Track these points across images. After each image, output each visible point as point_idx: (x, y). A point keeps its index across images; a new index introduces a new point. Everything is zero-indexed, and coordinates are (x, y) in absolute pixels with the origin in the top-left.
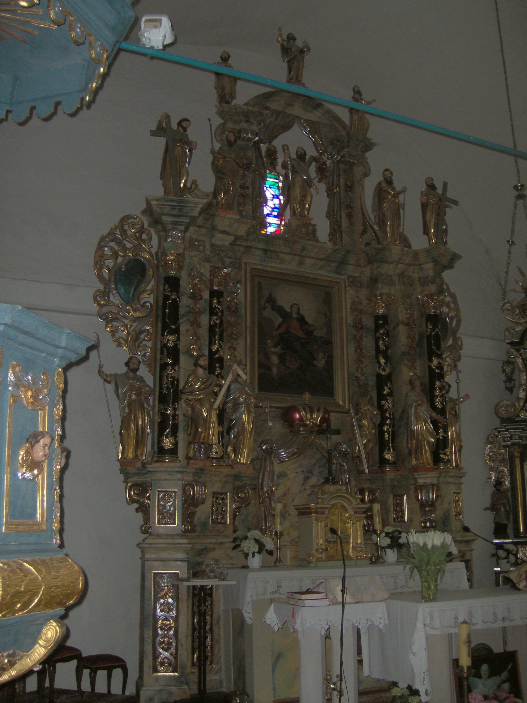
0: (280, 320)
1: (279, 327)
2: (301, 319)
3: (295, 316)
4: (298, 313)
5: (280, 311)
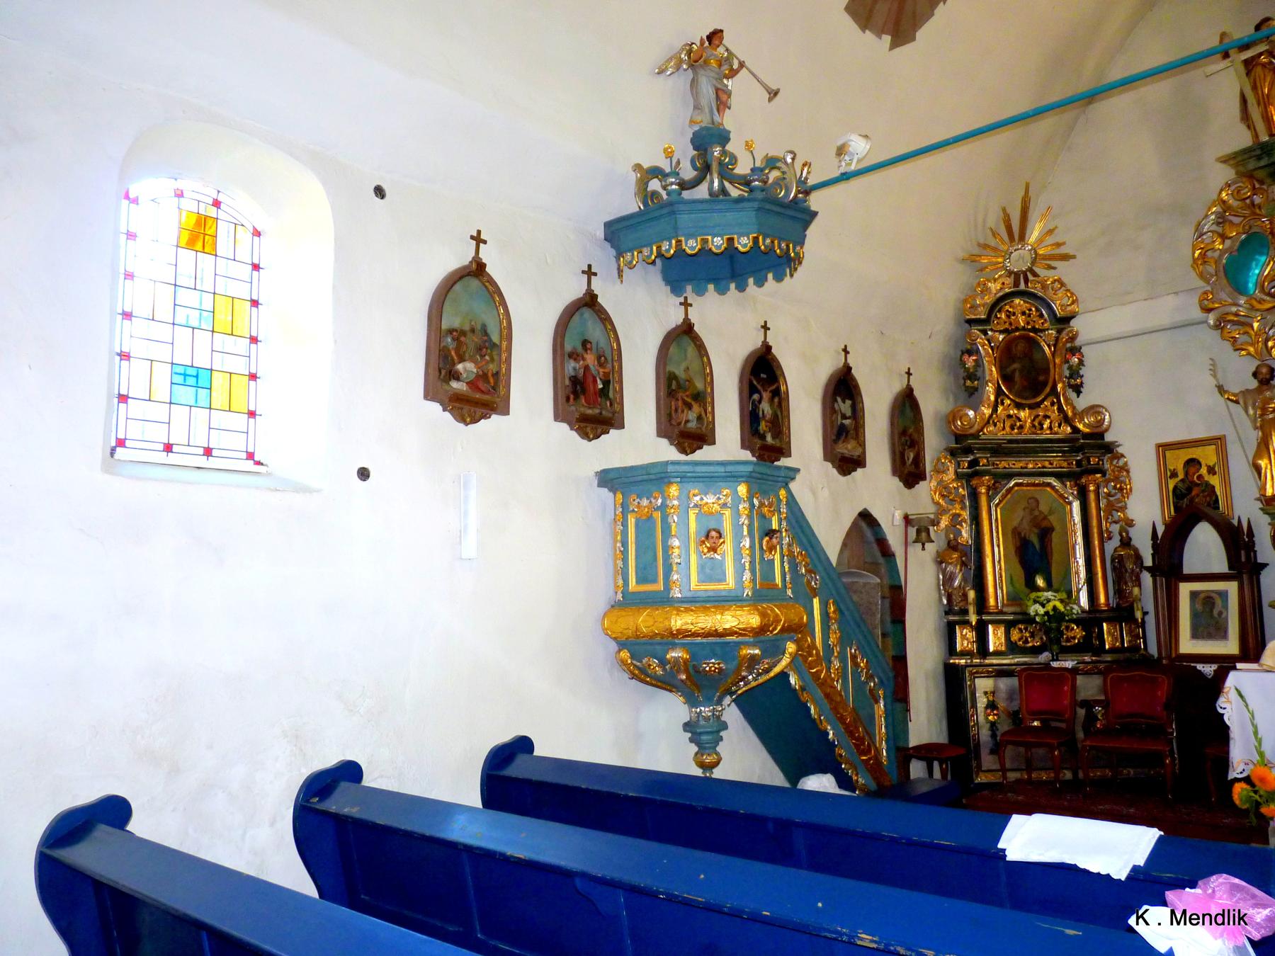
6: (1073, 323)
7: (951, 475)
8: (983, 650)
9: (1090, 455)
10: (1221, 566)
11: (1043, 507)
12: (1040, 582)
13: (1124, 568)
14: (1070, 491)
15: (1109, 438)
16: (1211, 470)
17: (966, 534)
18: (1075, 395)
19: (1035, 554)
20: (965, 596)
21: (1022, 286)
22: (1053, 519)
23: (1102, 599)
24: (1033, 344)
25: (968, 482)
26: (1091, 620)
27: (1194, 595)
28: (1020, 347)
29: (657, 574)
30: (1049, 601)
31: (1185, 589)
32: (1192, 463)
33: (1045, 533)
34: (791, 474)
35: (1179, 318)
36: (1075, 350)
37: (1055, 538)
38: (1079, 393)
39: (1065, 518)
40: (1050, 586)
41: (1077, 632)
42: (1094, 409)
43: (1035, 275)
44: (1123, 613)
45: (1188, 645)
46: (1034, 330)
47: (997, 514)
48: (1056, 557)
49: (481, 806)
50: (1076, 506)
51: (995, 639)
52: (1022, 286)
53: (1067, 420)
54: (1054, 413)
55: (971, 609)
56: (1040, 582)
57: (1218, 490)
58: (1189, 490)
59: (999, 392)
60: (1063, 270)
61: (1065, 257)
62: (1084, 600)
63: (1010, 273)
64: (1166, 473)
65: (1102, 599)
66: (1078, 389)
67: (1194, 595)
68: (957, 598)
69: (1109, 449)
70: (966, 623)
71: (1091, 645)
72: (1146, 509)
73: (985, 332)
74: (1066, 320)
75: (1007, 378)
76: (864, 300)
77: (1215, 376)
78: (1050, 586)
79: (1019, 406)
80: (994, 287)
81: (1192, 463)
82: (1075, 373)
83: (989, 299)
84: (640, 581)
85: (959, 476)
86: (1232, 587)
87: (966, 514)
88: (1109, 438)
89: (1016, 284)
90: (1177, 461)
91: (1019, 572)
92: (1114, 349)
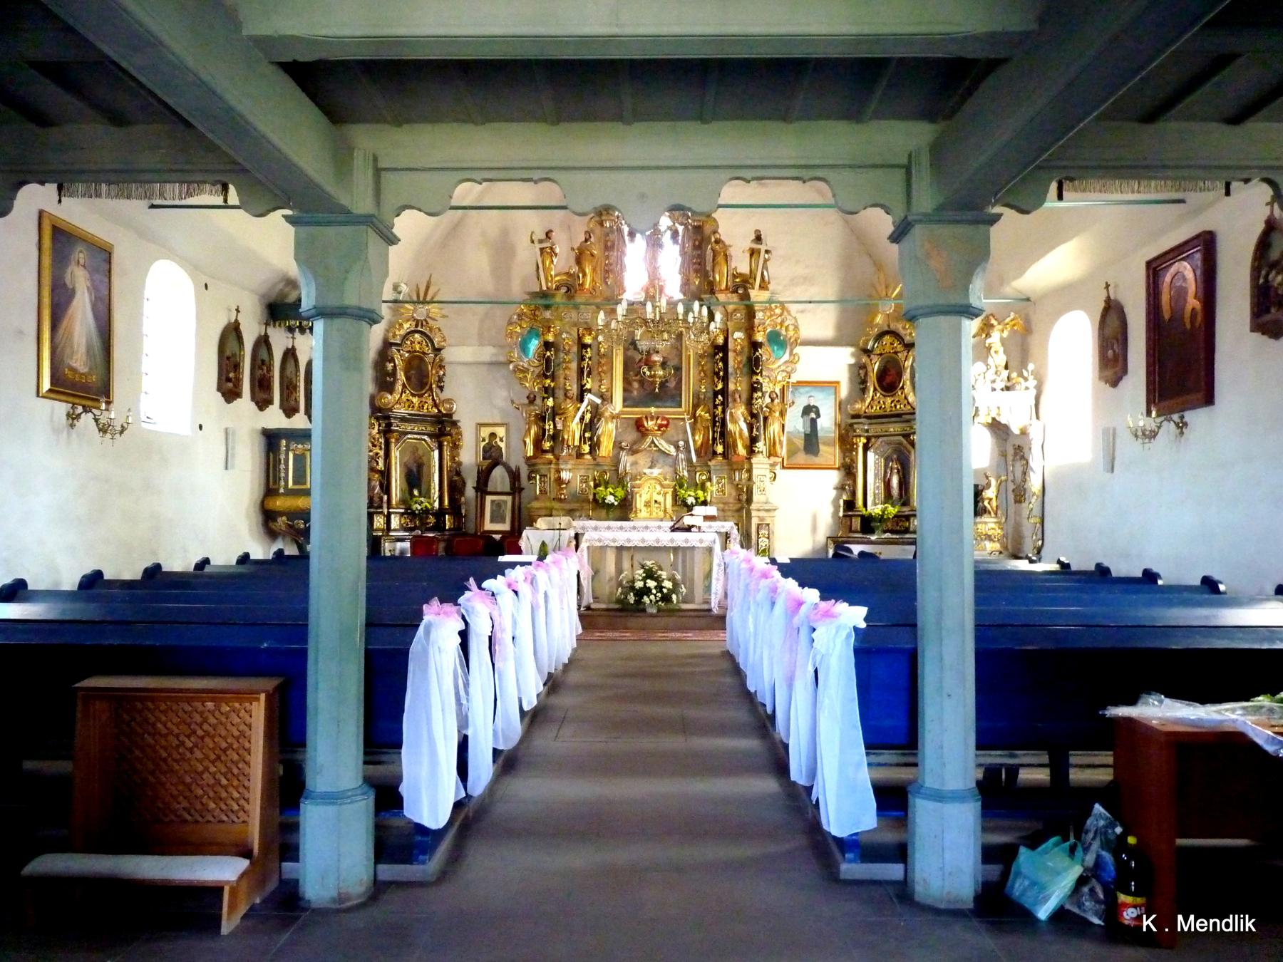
7: (376, 430)
8: (389, 528)
9: (443, 427)
10: (508, 489)
11: (420, 452)
12: (416, 493)
13: (456, 488)
14: (434, 445)
15: (455, 418)
16: (501, 440)
17: (381, 466)
19: (415, 478)
20: (381, 499)
22: (425, 459)
23: (446, 503)
24: (421, 359)
26: (440, 514)
27: (493, 502)
28: (416, 362)
31: (489, 499)
32: (493, 435)
33: (420, 466)
34: (368, 758)
35: (494, 359)
36: (442, 367)
37: (425, 469)
39: (430, 459)
40: (420, 495)
41: (432, 520)
42: (450, 401)
44: (455, 508)
45: (488, 526)
46: (424, 353)
47: (398, 454)
48: (424, 480)
49: (719, 215)
50: (436, 452)
51: (395, 522)
53: (436, 405)
54: (430, 401)
55: (385, 506)
56: (416, 493)
59: (404, 386)
62: (436, 505)
64: (478, 439)
65: (446, 503)
66: (441, 388)
67: (493, 502)
68: (376, 499)
69: (454, 424)
71: (439, 526)
72: (469, 456)
74: (439, 350)
75: (408, 378)
76: (362, 177)
78: (420, 495)
79: (413, 395)
80: (406, 326)
81: (493, 435)
82: (440, 380)
83: (402, 332)
84: (295, 483)
85: (379, 432)
86: (509, 499)
87: (382, 453)
88: (455, 418)
90: (485, 432)
91: (405, 486)
92: (459, 369)
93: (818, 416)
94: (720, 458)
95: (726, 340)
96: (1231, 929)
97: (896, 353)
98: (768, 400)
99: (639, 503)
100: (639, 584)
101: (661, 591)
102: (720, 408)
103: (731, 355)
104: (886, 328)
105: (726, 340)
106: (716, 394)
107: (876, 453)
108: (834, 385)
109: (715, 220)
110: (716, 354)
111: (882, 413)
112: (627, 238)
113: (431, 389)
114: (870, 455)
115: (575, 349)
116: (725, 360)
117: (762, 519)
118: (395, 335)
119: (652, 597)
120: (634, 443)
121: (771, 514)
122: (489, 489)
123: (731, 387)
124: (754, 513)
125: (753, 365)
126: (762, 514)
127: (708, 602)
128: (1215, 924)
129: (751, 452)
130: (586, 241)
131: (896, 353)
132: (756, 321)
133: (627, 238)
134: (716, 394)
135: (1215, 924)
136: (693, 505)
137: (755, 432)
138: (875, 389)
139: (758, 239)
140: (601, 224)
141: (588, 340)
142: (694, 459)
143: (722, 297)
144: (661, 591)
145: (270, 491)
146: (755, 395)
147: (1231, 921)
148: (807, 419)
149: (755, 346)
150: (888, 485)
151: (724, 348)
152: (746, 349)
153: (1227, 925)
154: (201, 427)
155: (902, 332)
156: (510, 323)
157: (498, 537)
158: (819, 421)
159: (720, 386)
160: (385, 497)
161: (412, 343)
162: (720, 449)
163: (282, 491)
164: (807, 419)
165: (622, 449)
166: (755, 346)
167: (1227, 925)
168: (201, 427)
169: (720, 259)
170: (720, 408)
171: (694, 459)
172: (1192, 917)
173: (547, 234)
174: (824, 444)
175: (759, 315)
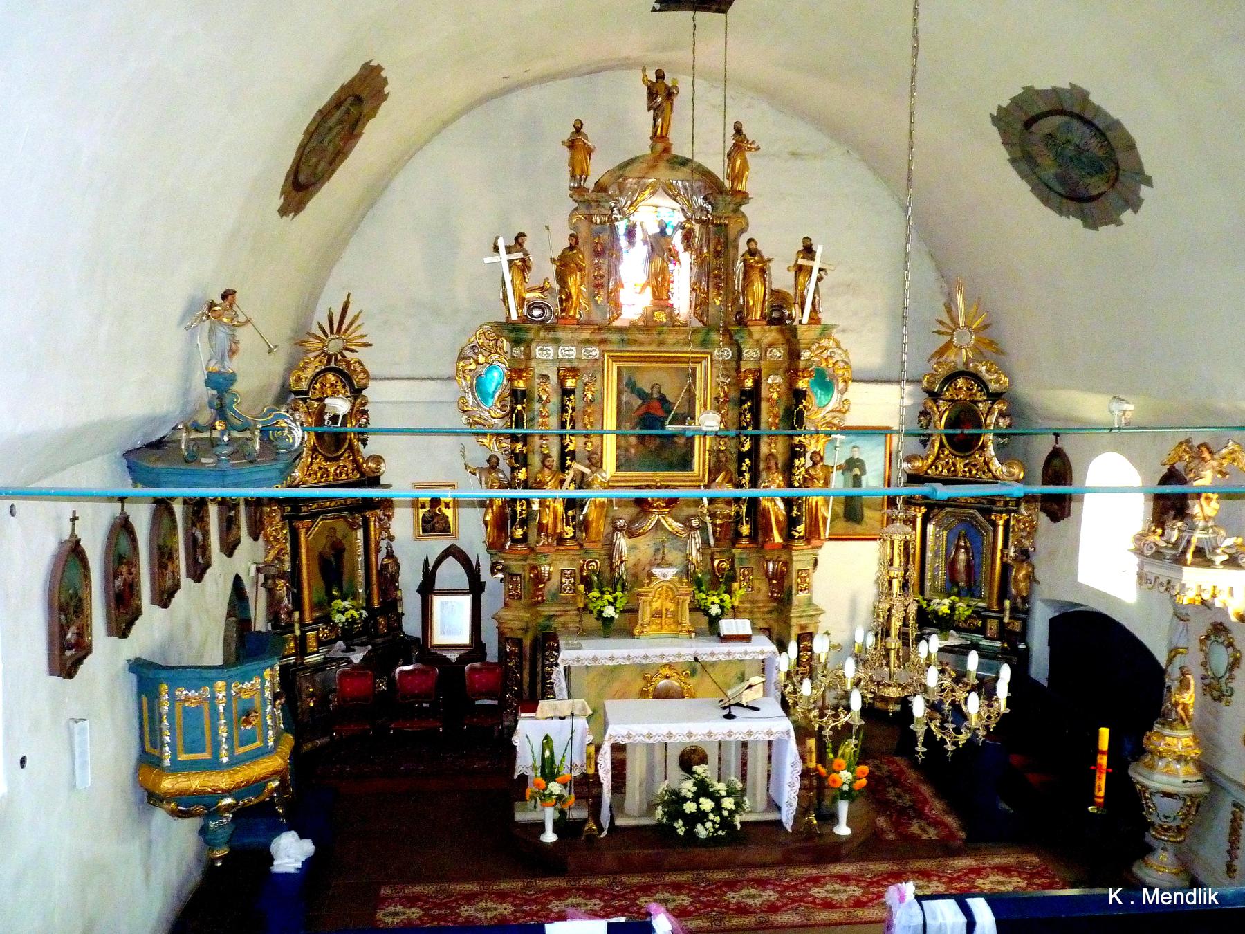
0: (640, 402)
1: (639, 407)
2: (663, 399)
3: (655, 396)
4: (659, 392)
5: (641, 394)
6: (364, 392)
11: (339, 535)
18: (361, 446)
21: (333, 364)
23: (376, 601)
25: (290, 523)
29: (1098, 896)
30: (346, 610)
36: (365, 412)
37: (346, 555)
38: (365, 445)
42: (378, 459)
43: (343, 356)
50: (360, 534)
52: (333, 364)
55: (297, 626)
57: (450, 520)
58: (433, 517)
60: (362, 354)
61: (365, 345)
63: (326, 354)
65: (376, 601)
70: (713, 811)
73: (305, 401)
74: (360, 390)
77: (464, 456)
79: (327, 459)
89: (329, 361)
93: (863, 472)
94: (744, 542)
95: (757, 383)
96: (1194, 902)
97: (975, 402)
98: (809, 463)
99: (645, 614)
100: (690, 807)
101: (721, 816)
102: (747, 476)
103: (764, 405)
104: (960, 367)
105: (757, 383)
106: (741, 457)
107: (937, 525)
108: (883, 432)
109: (744, 216)
110: (744, 402)
111: (950, 476)
112: (623, 242)
113: (351, 444)
114: (931, 528)
115: (555, 399)
116: (755, 411)
117: (803, 627)
118: (299, 379)
119: (709, 825)
120: (632, 522)
121: (814, 620)
122: (437, 587)
123: (764, 449)
124: (794, 621)
125: (794, 415)
126: (803, 621)
127: (774, 806)
128: (1179, 897)
129: (789, 537)
130: (571, 248)
131: (975, 402)
132: (802, 365)
133: (623, 242)
134: (741, 457)
135: (1179, 897)
136: (718, 618)
137: (795, 512)
138: (942, 446)
139: (808, 251)
140: (589, 217)
141: (570, 383)
142: (712, 542)
143: (756, 330)
144: (721, 816)
145: (148, 761)
146: (797, 462)
147: (1194, 894)
148: (849, 475)
149: (799, 395)
150: (951, 565)
151: (754, 395)
152: (784, 398)
153: (1191, 898)
154: (23, 762)
155: (987, 377)
156: (461, 358)
157: (453, 656)
158: (864, 478)
159: (747, 447)
160: (297, 615)
161: (323, 385)
162: (745, 530)
163: (167, 763)
164: (849, 475)
165: (616, 529)
166: (799, 395)
167: (1191, 898)
168: (23, 762)
169: (756, 276)
170: (747, 476)
171: (712, 542)
172: (1157, 891)
173: (516, 239)
174: (870, 507)
175: (806, 355)
